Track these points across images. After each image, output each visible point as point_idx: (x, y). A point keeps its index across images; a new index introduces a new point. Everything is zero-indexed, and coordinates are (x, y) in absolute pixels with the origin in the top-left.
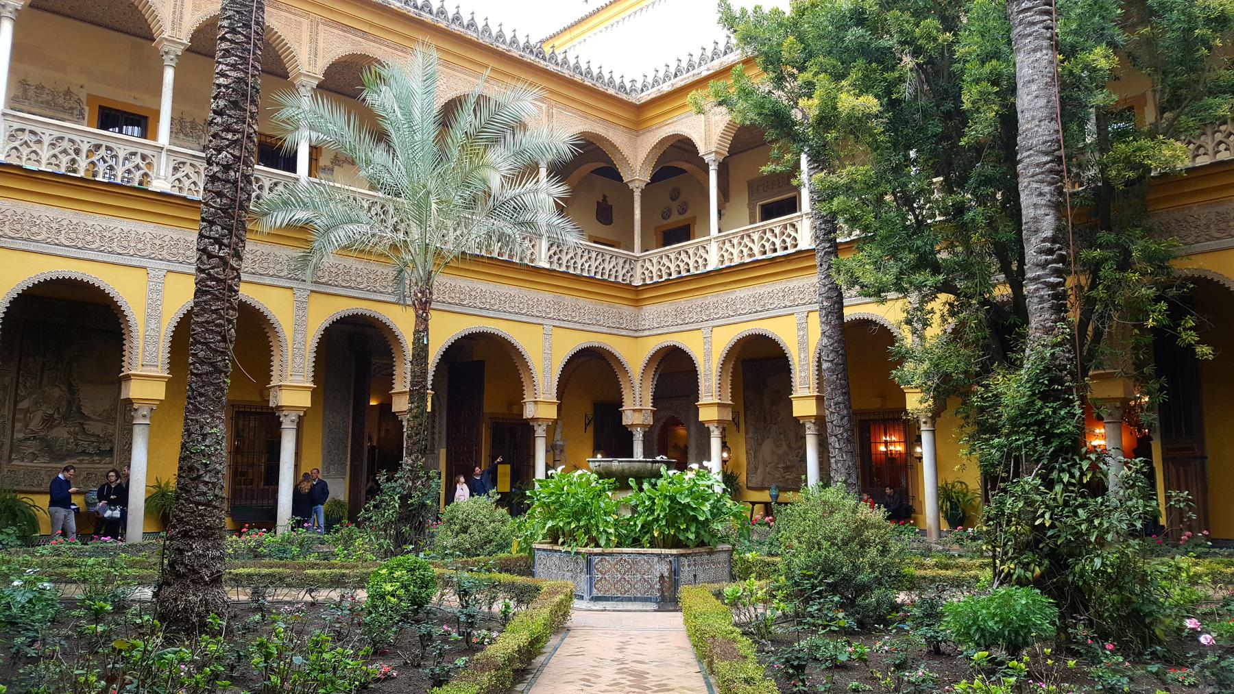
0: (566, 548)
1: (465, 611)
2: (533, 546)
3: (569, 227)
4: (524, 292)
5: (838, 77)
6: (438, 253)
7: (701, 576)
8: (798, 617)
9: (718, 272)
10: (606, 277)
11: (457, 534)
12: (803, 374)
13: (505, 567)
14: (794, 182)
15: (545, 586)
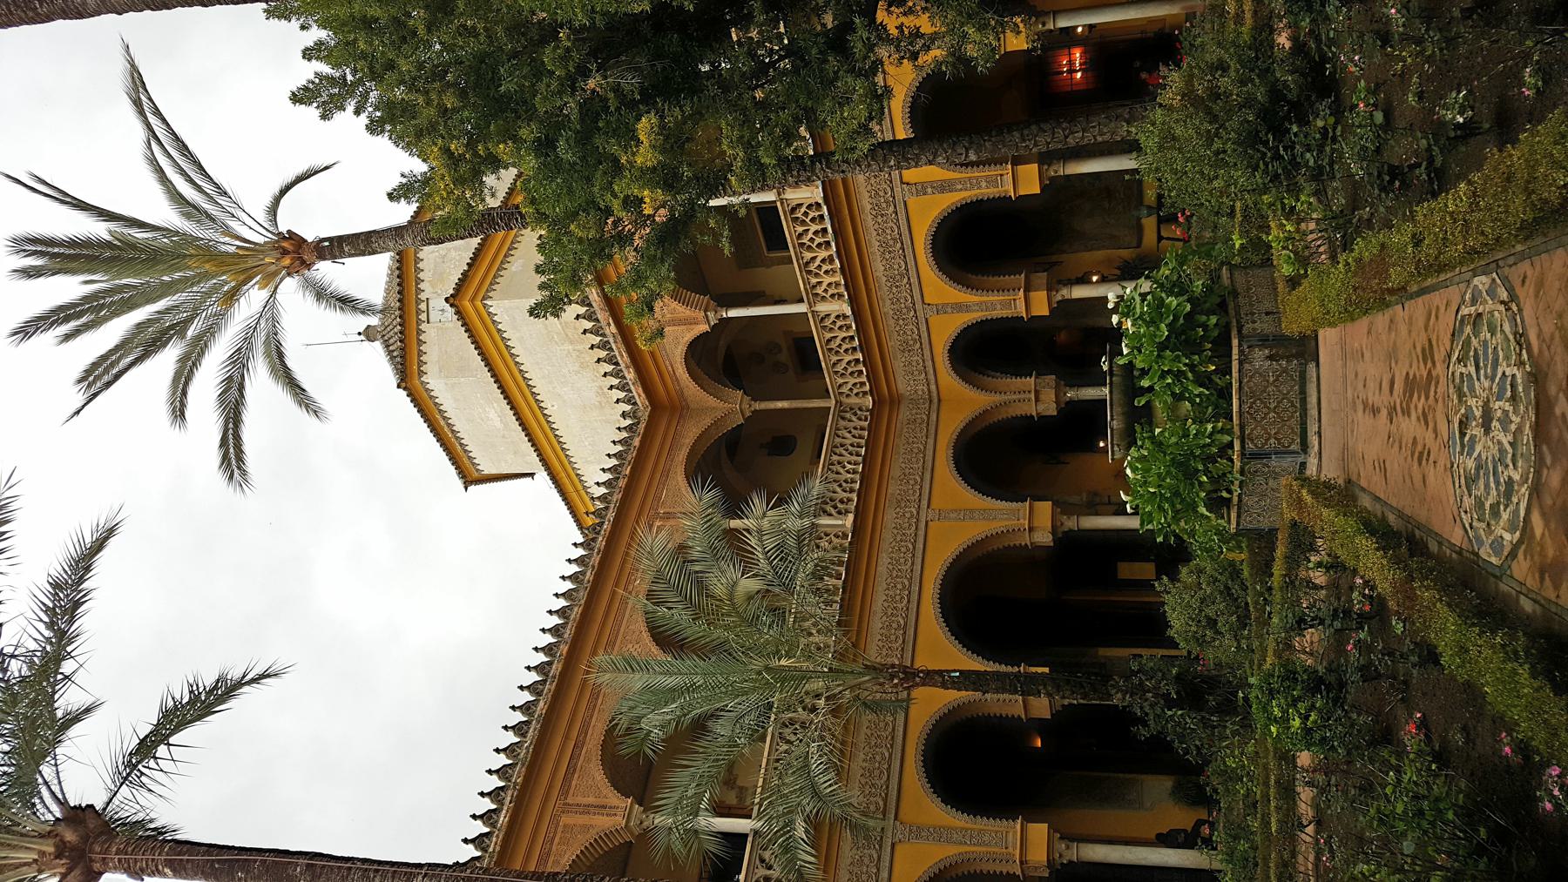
0: (1236, 488)
1: (1328, 622)
2: (1233, 531)
3: (802, 490)
4: (885, 546)
5: (617, 168)
6: (840, 656)
7: (1267, 305)
8: (1318, 175)
9: (854, 301)
10: (863, 442)
11: (1218, 632)
12: (984, 184)
13: (1264, 569)
14: (743, 213)
15: (1289, 514)
